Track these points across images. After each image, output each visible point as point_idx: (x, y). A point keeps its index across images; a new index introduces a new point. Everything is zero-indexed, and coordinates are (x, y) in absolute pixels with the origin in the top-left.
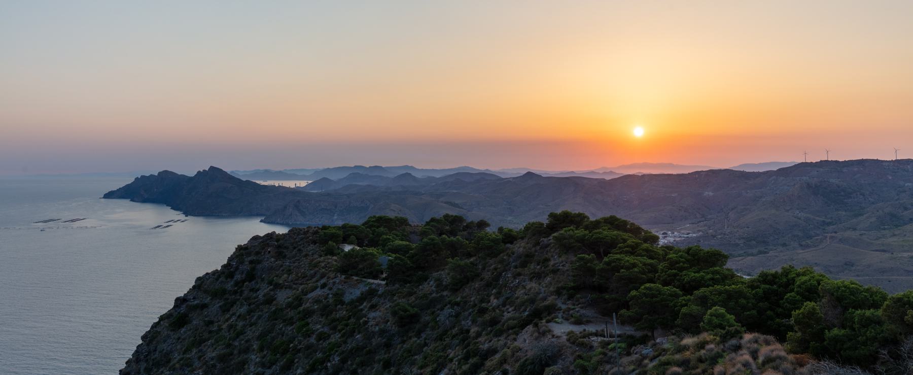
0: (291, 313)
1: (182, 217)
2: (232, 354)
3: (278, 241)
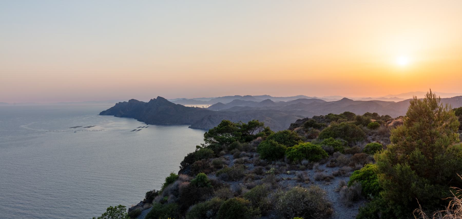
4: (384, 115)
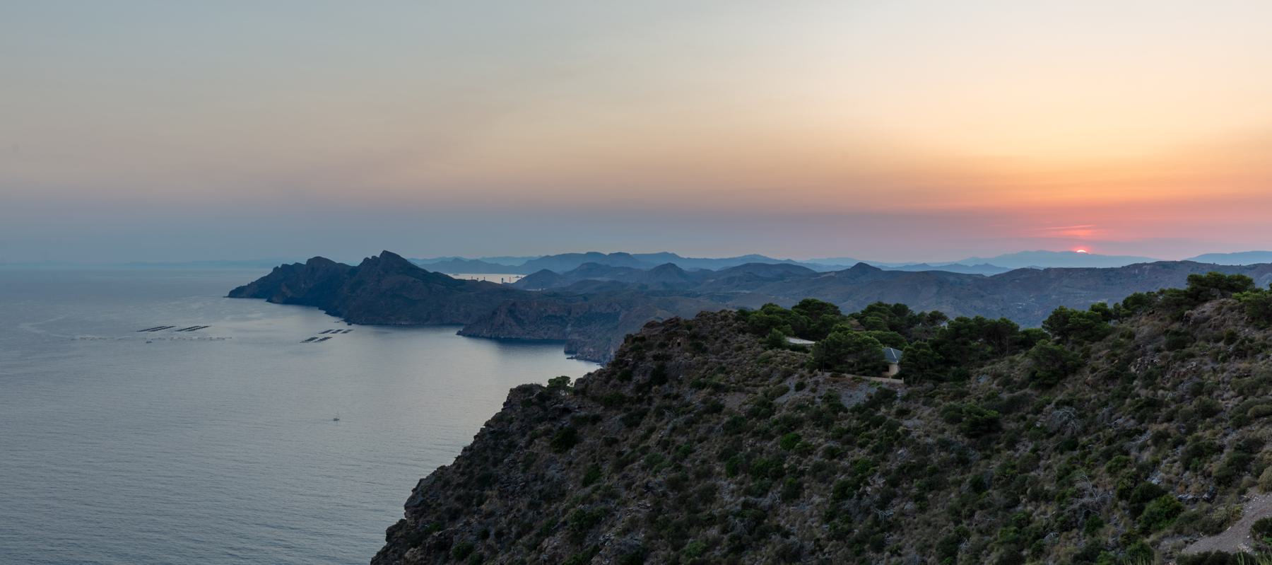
0: (762, 425)
1: (344, 326)
2: (686, 479)
3: (689, 328)
4: (928, 312)
